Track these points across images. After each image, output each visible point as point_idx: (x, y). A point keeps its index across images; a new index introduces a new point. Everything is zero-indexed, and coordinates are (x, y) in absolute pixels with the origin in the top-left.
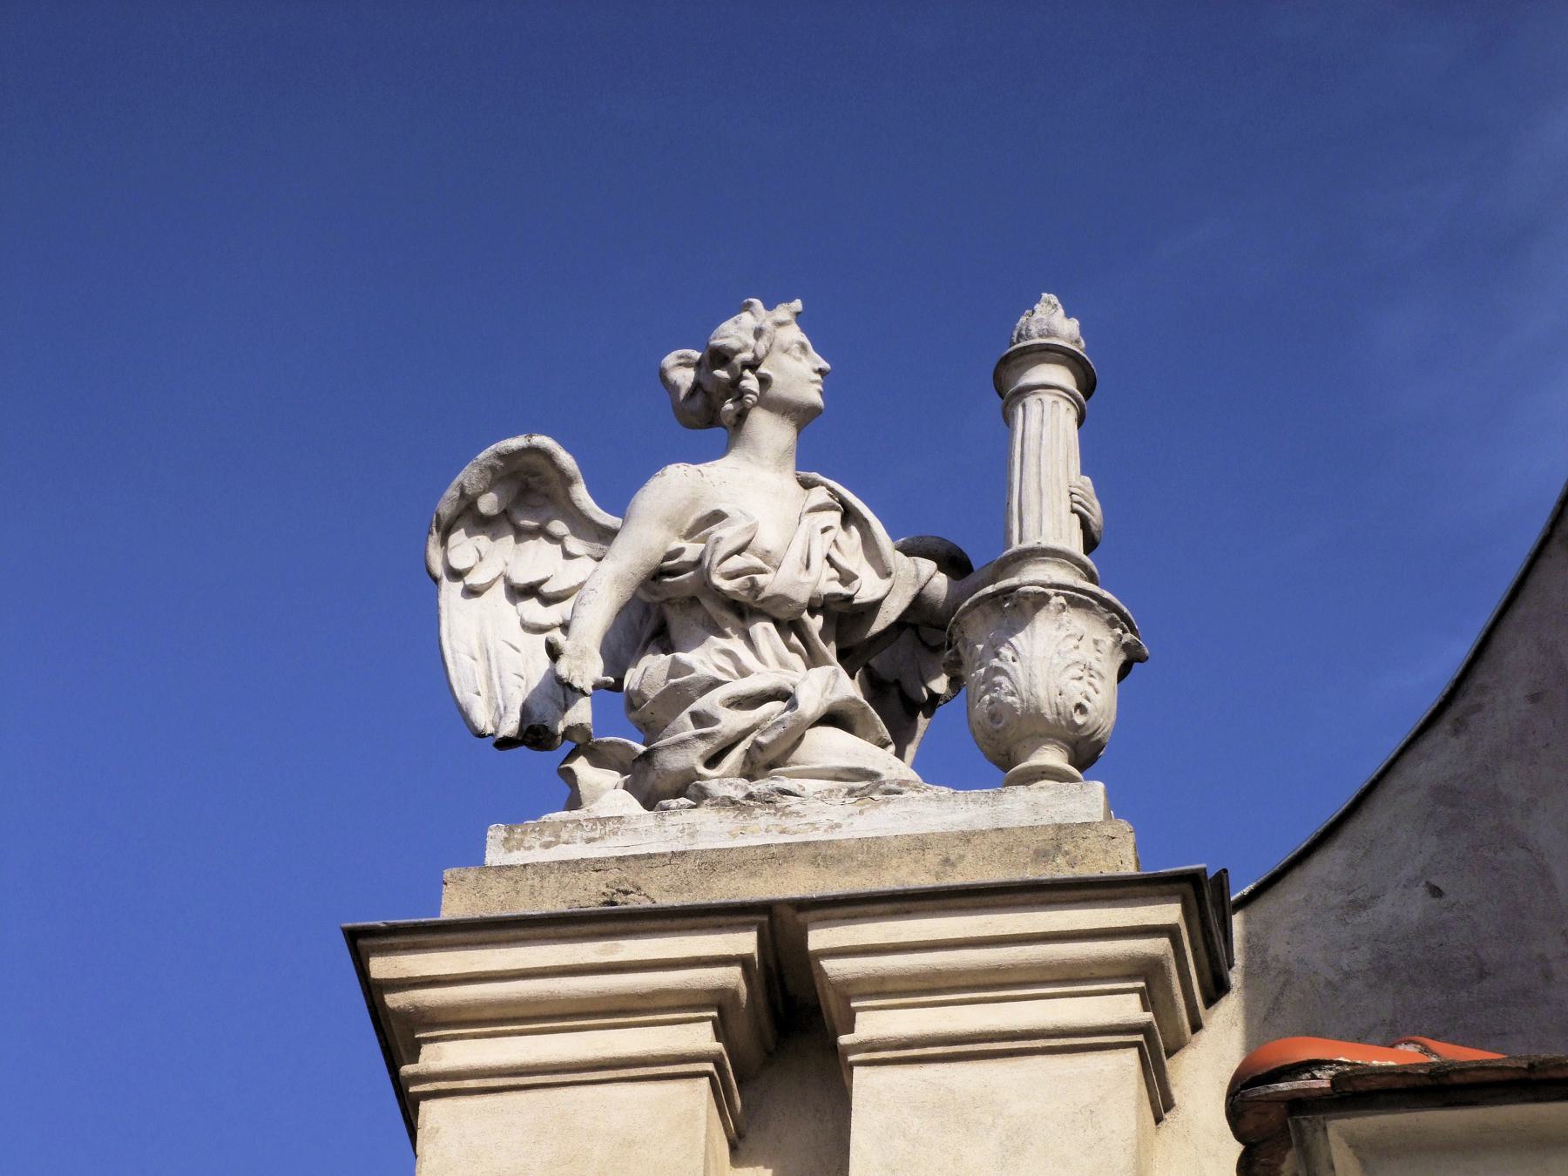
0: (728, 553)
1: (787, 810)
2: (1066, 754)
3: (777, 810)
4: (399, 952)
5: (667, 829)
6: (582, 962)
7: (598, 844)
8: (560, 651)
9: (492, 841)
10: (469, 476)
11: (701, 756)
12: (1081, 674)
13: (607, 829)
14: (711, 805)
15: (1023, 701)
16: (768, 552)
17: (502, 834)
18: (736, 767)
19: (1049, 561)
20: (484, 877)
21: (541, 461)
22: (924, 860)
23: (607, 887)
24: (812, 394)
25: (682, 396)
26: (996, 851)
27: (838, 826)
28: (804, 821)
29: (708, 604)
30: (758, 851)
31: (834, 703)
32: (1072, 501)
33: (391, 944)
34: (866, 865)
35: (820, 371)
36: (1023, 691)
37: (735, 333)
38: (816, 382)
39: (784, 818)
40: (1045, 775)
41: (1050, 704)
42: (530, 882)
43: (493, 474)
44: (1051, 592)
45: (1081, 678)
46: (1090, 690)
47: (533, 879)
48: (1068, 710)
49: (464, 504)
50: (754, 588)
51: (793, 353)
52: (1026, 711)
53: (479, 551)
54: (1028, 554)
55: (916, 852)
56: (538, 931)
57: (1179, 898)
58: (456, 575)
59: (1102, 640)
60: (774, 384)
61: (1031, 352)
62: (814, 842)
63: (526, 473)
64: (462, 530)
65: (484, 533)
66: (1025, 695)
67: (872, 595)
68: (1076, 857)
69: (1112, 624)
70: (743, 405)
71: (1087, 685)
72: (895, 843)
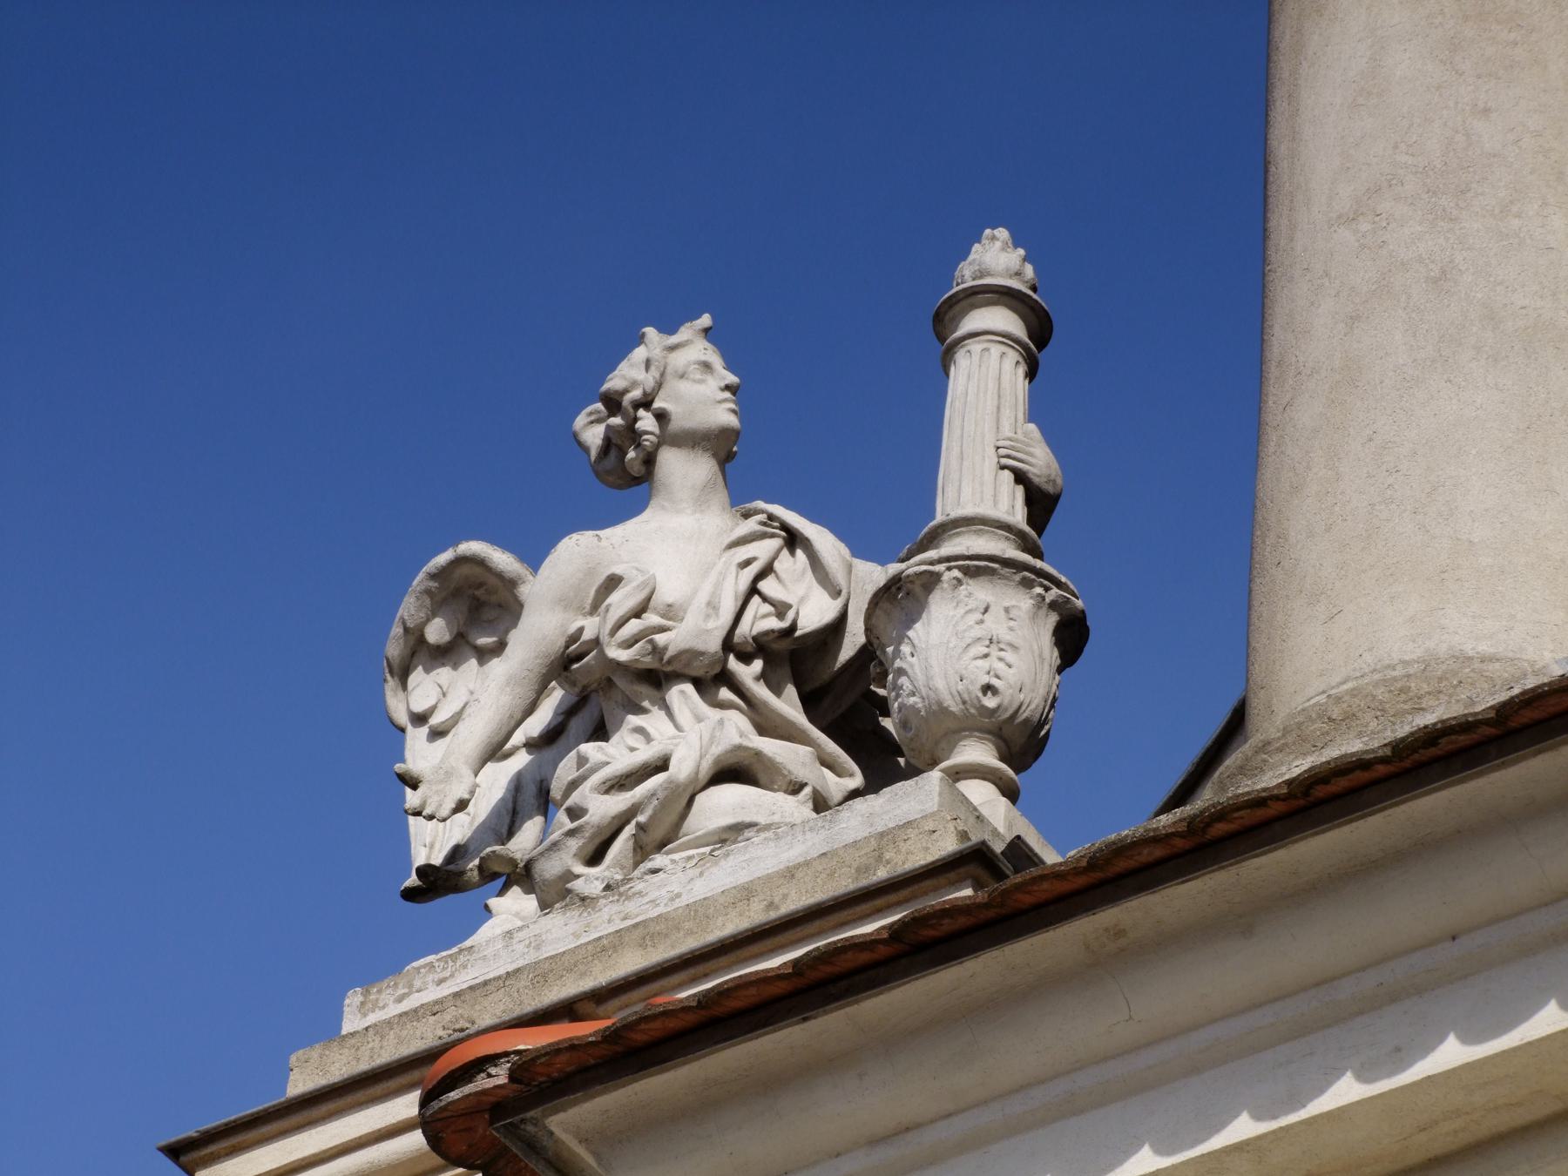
0: (619, 620)
1: (630, 893)
2: (991, 745)
3: (621, 895)
4: (222, 1159)
5: (514, 948)
6: (394, 1121)
7: (448, 983)
8: (417, 779)
9: (349, 1008)
10: (409, 608)
11: (575, 855)
12: (986, 650)
13: (458, 964)
14: (561, 908)
15: (923, 699)
16: (669, 606)
17: (359, 998)
18: (625, 857)
19: (963, 532)
20: (327, 1053)
21: (477, 570)
22: (748, 911)
23: (444, 1029)
24: (724, 415)
25: (594, 453)
26: (819, 880)
27: (678, 895)
28: (647, 899)
29: (620, 682)
30: (590, 947)
31: (719, 756)
32: (1000, 457)
33: (212, 1153)
34: (692, 933)
35: (727, 388)
36: (922, 688)
37: (629, 375)
38: (725, 400)
39: (626, 902)
40: (961, 775)
41: (951, 694)
42: (370, 1045)
43: (432, 599)
44: (940, 568)
45: (986, 656)
46: (1000, 666)
47: (373, 1041)
48: (973, 696)
49: (412, 640)
50: (656, 651)
51: (692, 376)
52: (928, 709)
53: (441, 687)
54: (939, 531)
55: (741, 904)
56: (349, 1099)
57: (969, 882)
58: (420, 719)
59: (1013, 606)
60: (673, 417)
61: (959, 301)
62: (643, 921)
63: (470, 587)
64: (420, 668)
65: (443, 665)
66: (924, 691)
67: (820, 621)
68: (896, 864)
69: (1027, 584)
70: (645, 449)
71: (997, 661)
72: (721, 900)
